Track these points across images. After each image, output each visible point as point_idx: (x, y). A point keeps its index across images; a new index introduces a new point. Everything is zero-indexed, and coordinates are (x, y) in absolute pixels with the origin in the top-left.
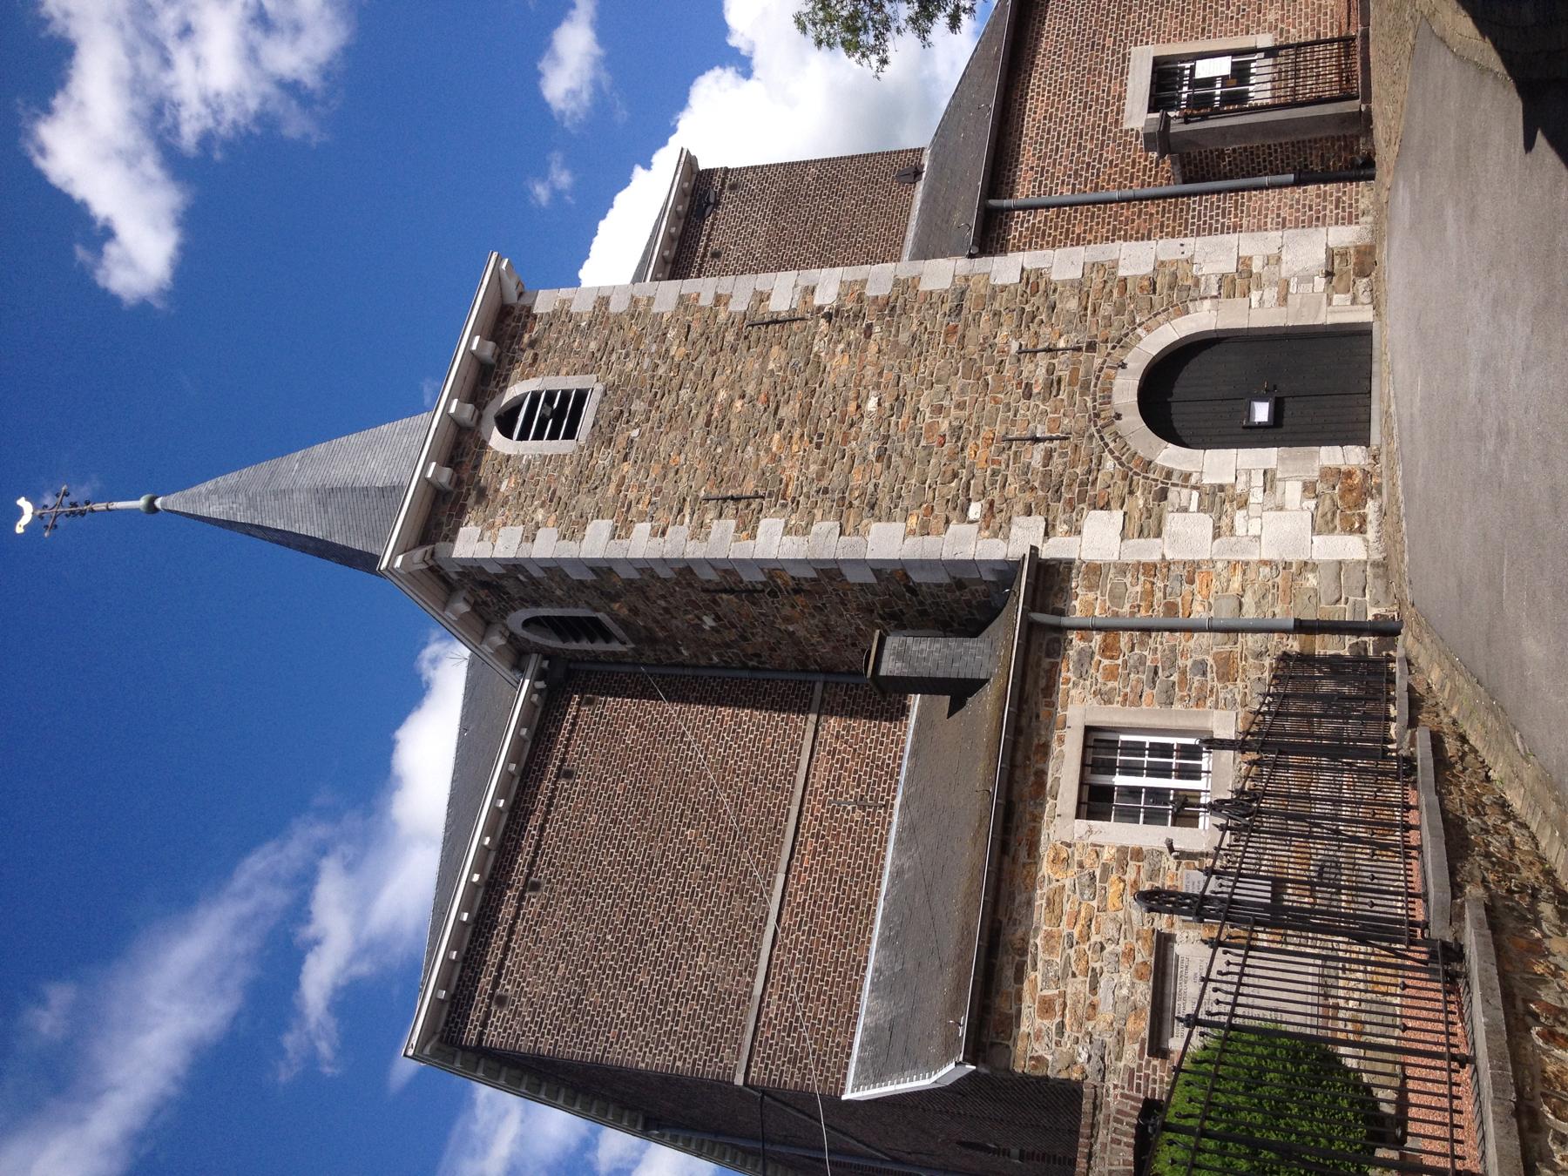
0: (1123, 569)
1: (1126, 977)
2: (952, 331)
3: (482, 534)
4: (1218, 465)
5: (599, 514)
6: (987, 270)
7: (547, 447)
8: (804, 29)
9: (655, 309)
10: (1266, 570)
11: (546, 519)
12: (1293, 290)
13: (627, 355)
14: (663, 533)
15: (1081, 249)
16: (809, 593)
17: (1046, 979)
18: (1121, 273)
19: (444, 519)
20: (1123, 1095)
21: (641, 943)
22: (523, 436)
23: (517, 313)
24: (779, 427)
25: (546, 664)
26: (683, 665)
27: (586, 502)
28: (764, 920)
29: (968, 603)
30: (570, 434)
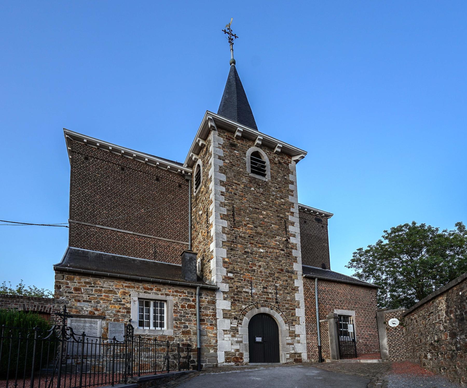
0: (214, 309)
1: (89, 309)
2: (282, 270)
3: (220, 144)
4: (244, 330)
5: (228, 178)
6: (299, 279)
7: (248, 165)
8: (358, 250)
9: (289, 196)
10: (214, 341)
11: (226, 163)
12: (291, 346)
13: (276, 188)
14: (222, 195)
15: (303, 300)
16: (207, 236)
17: (87, 289)
18: (296, 309)
19: (226, 134)
20: (51, 308)
21: (109, 197)
22: (252, 159)
23: (289, 159)
24: (255, 227)
25: (189, 174)
26: (191, 210)
27: (231, 174)
28: (119, 228)
29: (207, 275)
30: (252, 172)
